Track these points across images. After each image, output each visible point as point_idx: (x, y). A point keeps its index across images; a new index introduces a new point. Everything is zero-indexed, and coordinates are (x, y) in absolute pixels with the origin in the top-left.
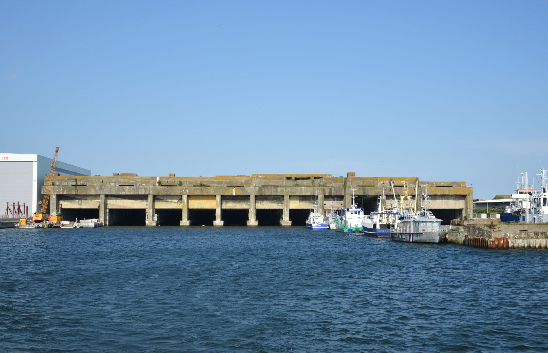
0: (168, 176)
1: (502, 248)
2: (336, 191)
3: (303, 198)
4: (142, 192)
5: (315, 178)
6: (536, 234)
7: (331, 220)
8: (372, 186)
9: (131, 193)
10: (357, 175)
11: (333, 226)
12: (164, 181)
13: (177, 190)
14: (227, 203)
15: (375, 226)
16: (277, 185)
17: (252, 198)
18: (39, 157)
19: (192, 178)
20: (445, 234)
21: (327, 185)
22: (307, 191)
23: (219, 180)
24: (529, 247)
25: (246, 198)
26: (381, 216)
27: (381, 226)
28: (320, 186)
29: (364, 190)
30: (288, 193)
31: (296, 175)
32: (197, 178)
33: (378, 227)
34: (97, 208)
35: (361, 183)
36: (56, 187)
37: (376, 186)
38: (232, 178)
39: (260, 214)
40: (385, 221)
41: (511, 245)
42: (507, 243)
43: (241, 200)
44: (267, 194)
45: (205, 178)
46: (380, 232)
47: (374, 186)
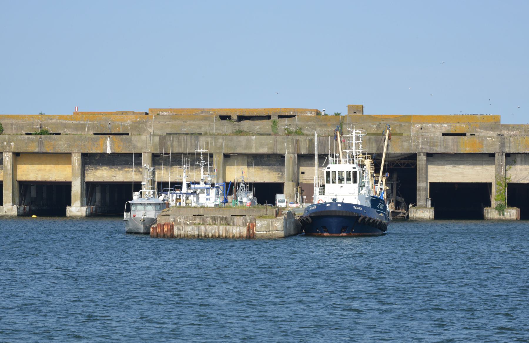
3: (257, 160)
5: (281, 117)
6: (214, 219)
10: (366, 112)
14: (96, 169)
16: (198, 131)
19: (23, 117)
21: (305, 132)
22: (262, 145)
25: (131, 159)
28: (289, 133)
30: (220, 148)
32: (33, 117)
38: (104, 117)
41: (176, 232)
42: (172, 229)
45: (49, 118)
47: (401, 134)
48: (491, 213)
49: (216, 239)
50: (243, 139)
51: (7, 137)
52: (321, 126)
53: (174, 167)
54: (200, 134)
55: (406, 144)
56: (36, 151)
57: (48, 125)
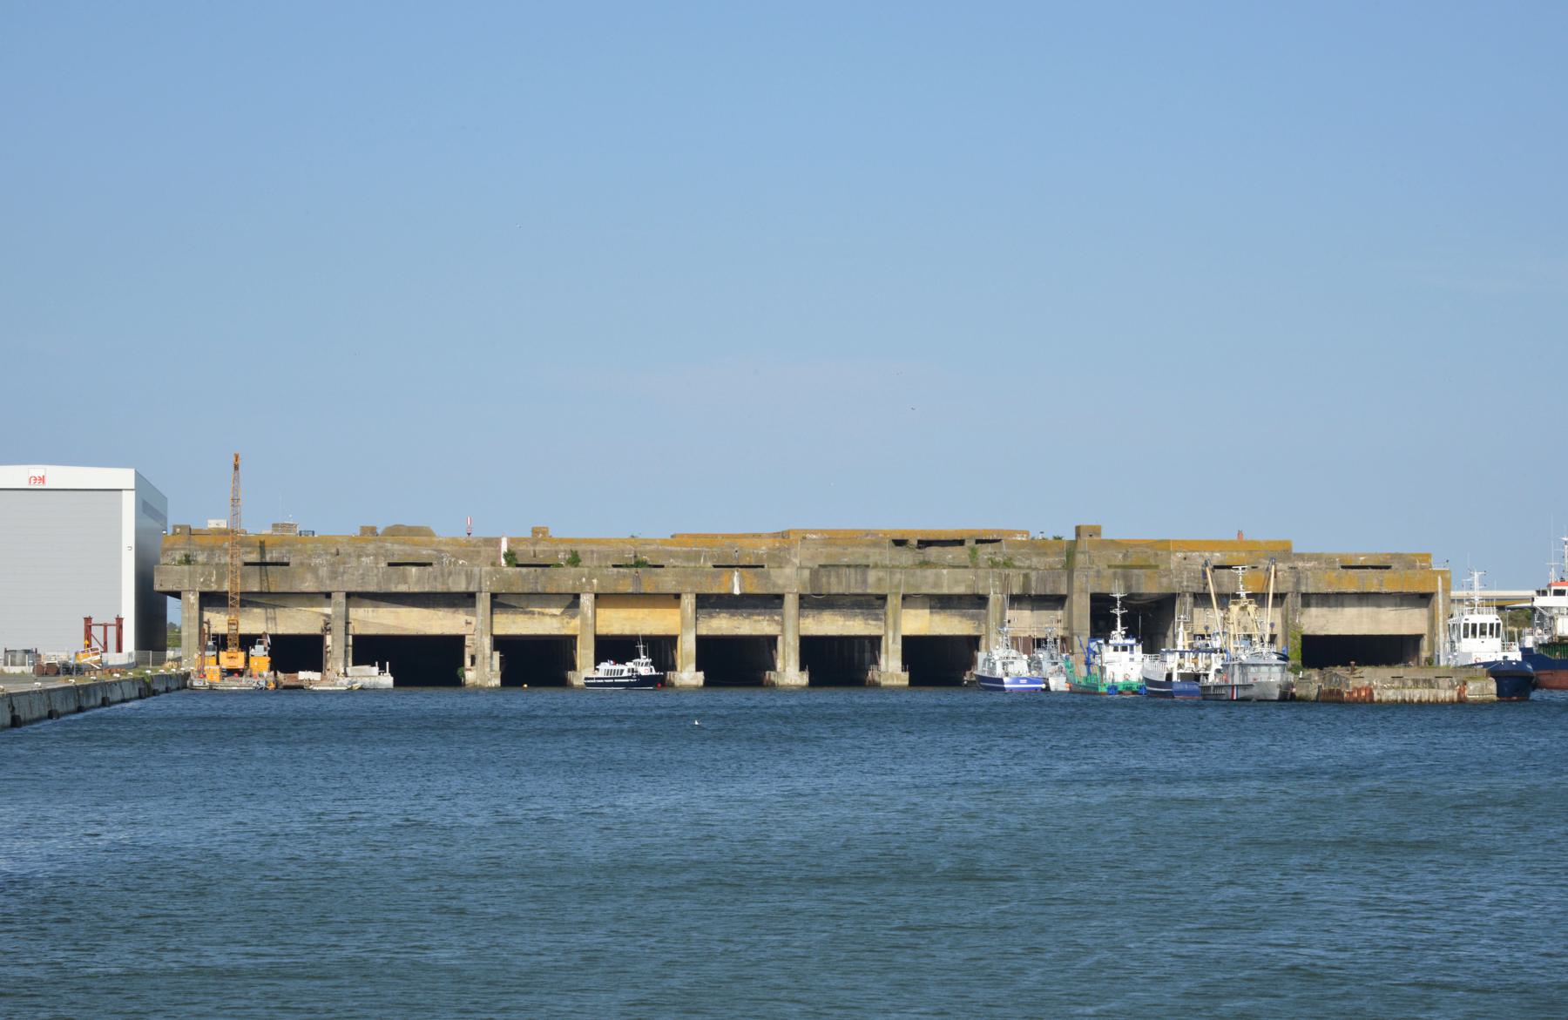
0: (529, 534)
1: (1364, 701)
2: (1042, 580)
3: (942, 602)
4: (460, 586)
5: (978, 542)
6: (1416, 682)
7: (1047, 667)
8: (1150, 567)
9: (427, 589)
10: (1105, 535)
11: (1058, 683)
12: (526, 551)
13: (565, 580)
15: (1169, 676)
16: (864, 562)
17: (791, 603)
18: (138, 477)
19: (608, 542)
20: (1291, 685)
21: (1017, 564)
22: (957, 582)
23: (691, 548)
24: (1404, 701)
25: (770, 602)
26: (1182, 656)
27: (1182, 676)
28: (995, 565)
29: (1126, 578)
30: (898, 586)
31: (922, 532)
32: (623, 541)
33: (1175, 678)
34: (318, 632)
35: (1119, 558)
36: (199, 569)
37: (1162, 567)
38: (727, 542)
39: (814, 651)
40: (1189, 667)
41: (1376, 697)
42: (1371, 694)
43: (755, 607)
44: (835, 590)
45: (646, 542)
46: (1180, 687)
47: (1156, 567)
48: (578, 678)
49: (1421, 704)
50: (930, 573)
51: (586, 570)
52: (1038, 555)
53: (806, 612)
54: (867, 566)
55: (1165, 581)
56: (630, 590)
57: (645, 553)
